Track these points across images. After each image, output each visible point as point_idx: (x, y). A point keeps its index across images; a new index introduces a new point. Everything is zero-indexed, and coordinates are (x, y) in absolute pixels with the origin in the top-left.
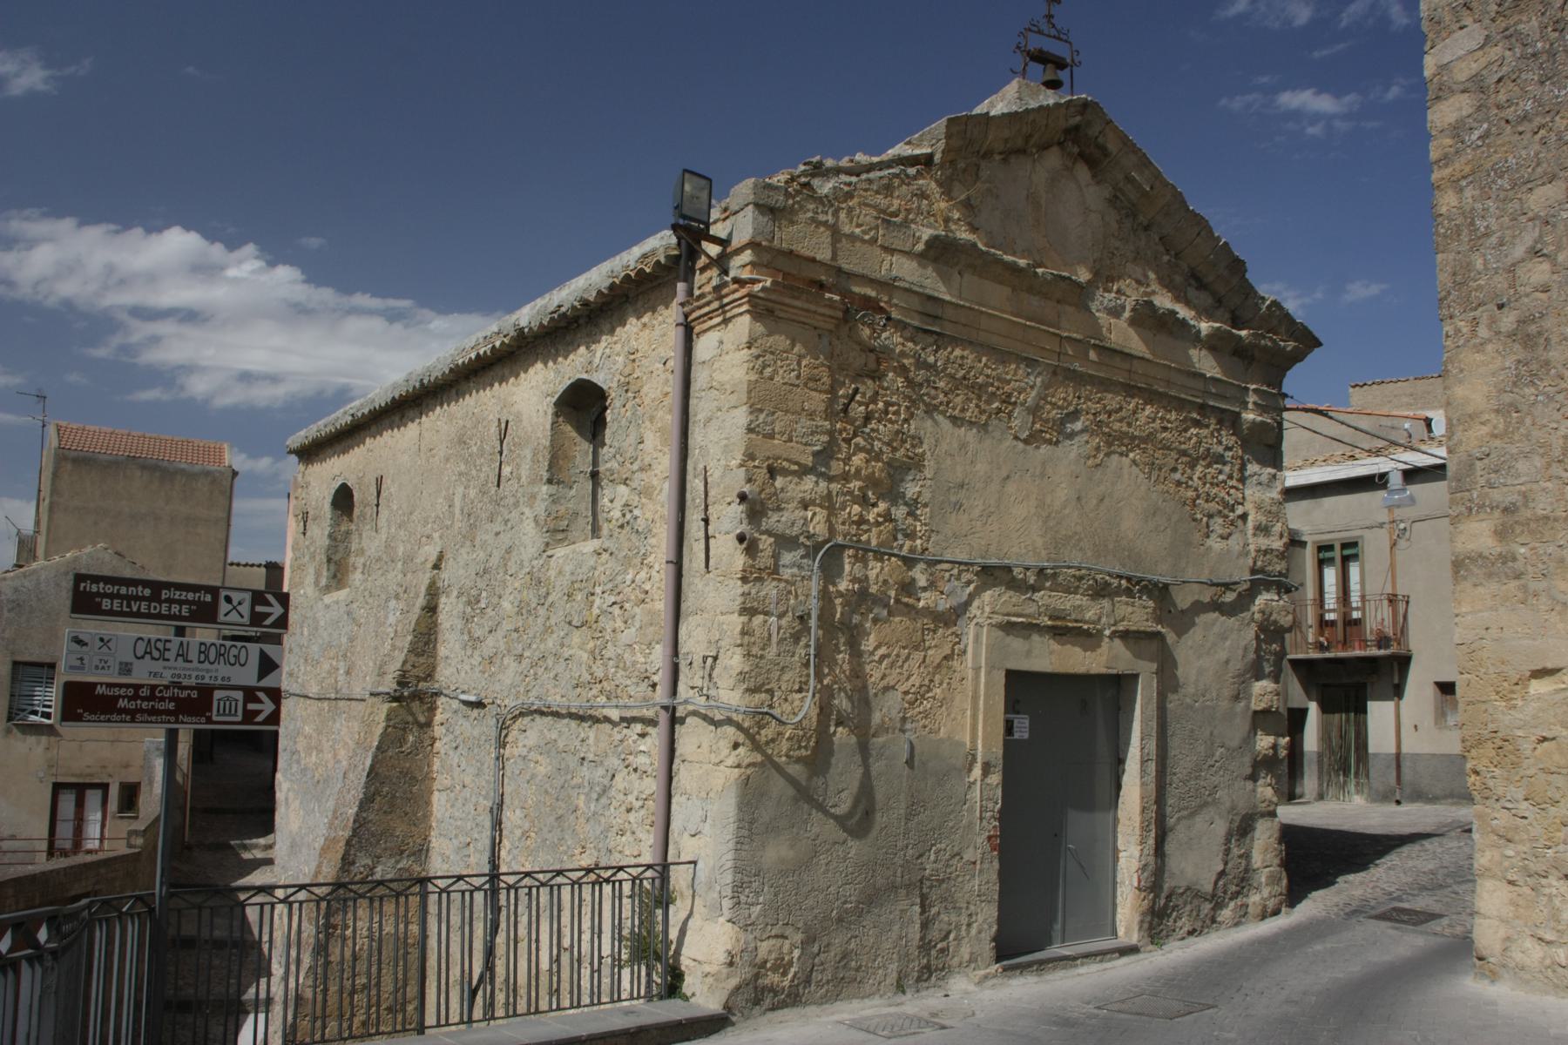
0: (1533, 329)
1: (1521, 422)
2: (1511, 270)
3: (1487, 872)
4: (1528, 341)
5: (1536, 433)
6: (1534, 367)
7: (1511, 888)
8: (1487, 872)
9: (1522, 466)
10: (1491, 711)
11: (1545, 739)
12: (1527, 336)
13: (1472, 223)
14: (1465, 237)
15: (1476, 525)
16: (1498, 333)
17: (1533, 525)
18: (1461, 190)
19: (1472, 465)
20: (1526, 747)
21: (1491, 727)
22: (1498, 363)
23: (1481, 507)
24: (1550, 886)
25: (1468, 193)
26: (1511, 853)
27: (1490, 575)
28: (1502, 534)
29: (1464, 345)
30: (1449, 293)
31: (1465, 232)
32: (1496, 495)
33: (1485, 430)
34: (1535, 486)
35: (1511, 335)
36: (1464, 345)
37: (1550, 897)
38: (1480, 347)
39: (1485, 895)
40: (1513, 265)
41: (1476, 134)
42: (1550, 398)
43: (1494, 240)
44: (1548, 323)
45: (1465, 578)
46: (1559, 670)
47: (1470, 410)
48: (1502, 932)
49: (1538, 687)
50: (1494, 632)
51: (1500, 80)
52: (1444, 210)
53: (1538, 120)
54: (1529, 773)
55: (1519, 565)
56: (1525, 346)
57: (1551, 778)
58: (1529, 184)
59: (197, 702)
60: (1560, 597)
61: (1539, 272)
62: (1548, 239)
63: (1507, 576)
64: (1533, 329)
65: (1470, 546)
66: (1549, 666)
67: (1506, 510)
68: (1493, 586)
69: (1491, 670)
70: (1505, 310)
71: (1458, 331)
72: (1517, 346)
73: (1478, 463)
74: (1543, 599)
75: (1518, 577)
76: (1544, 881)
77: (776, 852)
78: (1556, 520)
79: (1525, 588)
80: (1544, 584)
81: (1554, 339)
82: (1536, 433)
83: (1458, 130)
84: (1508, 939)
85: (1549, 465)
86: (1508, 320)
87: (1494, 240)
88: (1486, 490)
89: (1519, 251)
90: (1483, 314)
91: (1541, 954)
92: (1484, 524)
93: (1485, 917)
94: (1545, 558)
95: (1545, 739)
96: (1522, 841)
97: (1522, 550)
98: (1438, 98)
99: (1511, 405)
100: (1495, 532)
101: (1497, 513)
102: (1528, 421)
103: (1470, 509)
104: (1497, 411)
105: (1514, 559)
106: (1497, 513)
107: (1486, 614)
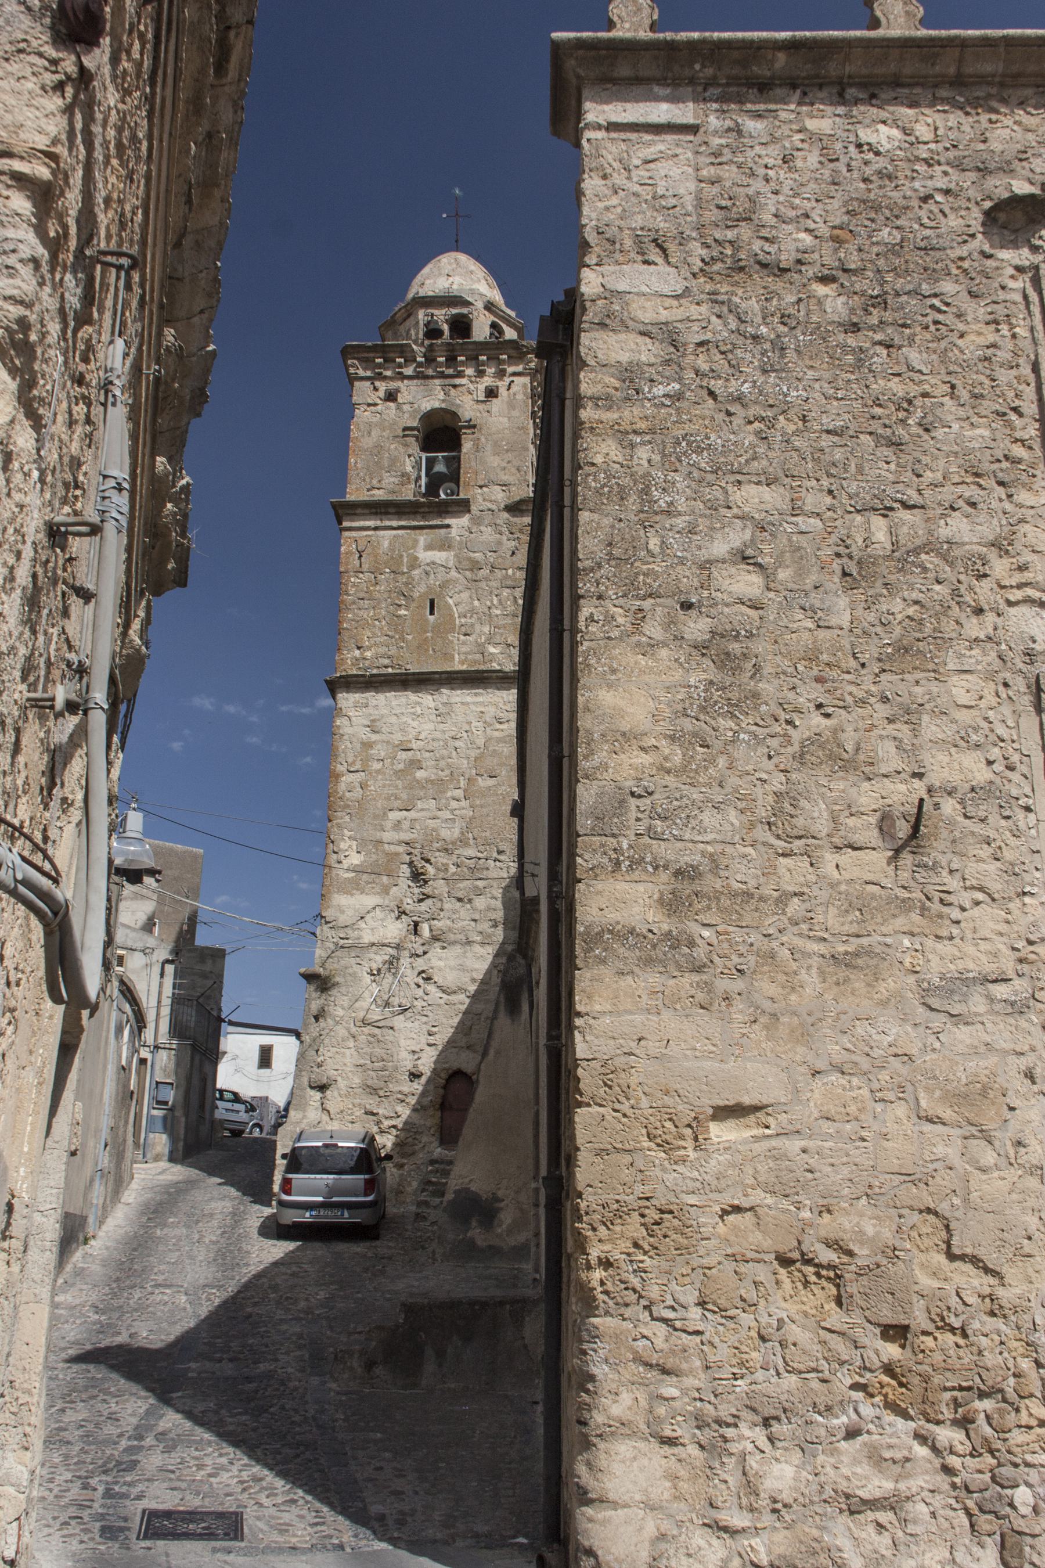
0: (735, 647)
1: (712, 761)
2: (706, 565)
3: (624, 1428)
4: (726, 661)
5: (733, 781)
6: (734, 695)
7: (667, 1450)
8: (624, 1428)
9: (709, 818)
10: (640, 1164)
11: (737, 1209)
12: (723, 651)
13: (646, 491)
14: (633, 501)
15: (621, 886)
16: (679, 638)
17: (726, 902)
18: (632, 446)
19: (622, 802)
20: (708, 1221)
21: (639, 1189)
22: (678, 675)
23: (637, 863)
24: (742, 1437)
25: (643, 454)
26: (674, 1392)
27: (648, 962)
28: (672, 904)
29: (620, 639)
30: (599, 566)
31: (633, 497)
32: (665, 851)
33: (646, 759)
34: (729, 849)
35: (701, 648)
36: (620, 639)
37: (743, 1456)
38: (650, 648)
39: (617, 1468)
40: (708, 561)
41: (660, 390)
42: (760, 741)
43: (680, 522)
44: (759, 647)
45: (603, 961)
46: (756, 1109)
47: (625, 726)
48: (650, 1529)
49: (720, 1132)
50: (653, 1046)
51: (701, 344)
52: (599, 460)
53: (754, 411)
54: (705, 1262)
55: (700, 952)
56: (721, 666)
57: (743, 1268)
58: (740, 477)
59: (790, 169)
60: (767, 1005)
61: (748, 583)
62: (766, 548)
63: (679, 967)
64: (735, 647)
65: (612, 916)
66: (747, 1100)
67: (678, 873)
68: (653, 979)
69: (645, 1103)
70: (693, 613)
71: (610, 618)
72: (707, 662)
73: (633, 802)
74: (739, 1004)
75: (698, 969)
76: (730, 1432)
77: (78, 1414)
78: (761, 899)
79: (708, 987)
80: (739, 985)
81: (768, 669)
82: (733, 781)
83: (630, 375)
84: (662, 1537)
85: (752, 826)
86: (697, 627)
87: (680, 522)
88: (646, 840)
89: (720, 548)
90: (658, 611)
91: (722, 1553)
92: (641, 887)
93: (615, 1505)
94: (743, 949)
95: (737, 1209)
96: (691, 1372)
97: (706, 933)
98: (602, 325)
99: (695, 735)
100: (661, 901)
101: (664, 876)
102: (722, 762)
103: (618, 864)
104: (672, 738)
105: (691, 944)
106: (664, 876)
107: (638, 1018)
